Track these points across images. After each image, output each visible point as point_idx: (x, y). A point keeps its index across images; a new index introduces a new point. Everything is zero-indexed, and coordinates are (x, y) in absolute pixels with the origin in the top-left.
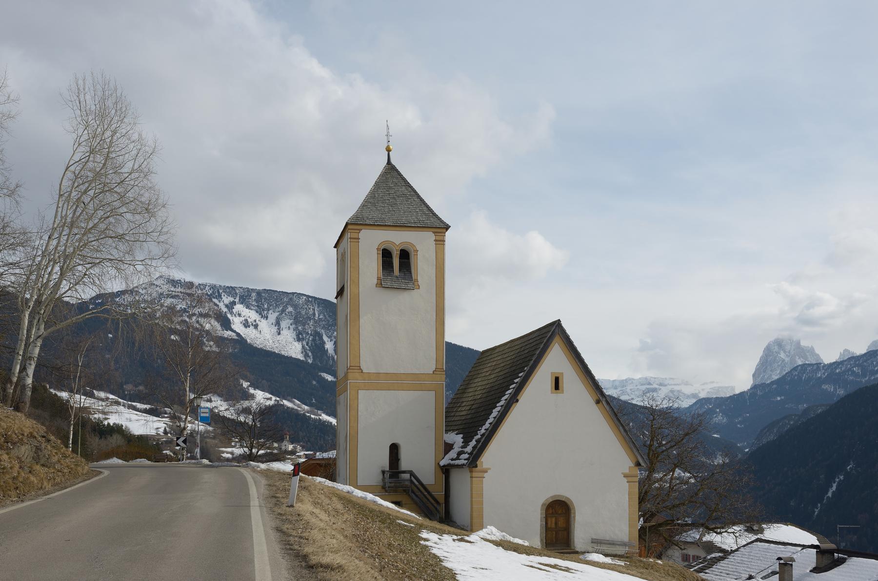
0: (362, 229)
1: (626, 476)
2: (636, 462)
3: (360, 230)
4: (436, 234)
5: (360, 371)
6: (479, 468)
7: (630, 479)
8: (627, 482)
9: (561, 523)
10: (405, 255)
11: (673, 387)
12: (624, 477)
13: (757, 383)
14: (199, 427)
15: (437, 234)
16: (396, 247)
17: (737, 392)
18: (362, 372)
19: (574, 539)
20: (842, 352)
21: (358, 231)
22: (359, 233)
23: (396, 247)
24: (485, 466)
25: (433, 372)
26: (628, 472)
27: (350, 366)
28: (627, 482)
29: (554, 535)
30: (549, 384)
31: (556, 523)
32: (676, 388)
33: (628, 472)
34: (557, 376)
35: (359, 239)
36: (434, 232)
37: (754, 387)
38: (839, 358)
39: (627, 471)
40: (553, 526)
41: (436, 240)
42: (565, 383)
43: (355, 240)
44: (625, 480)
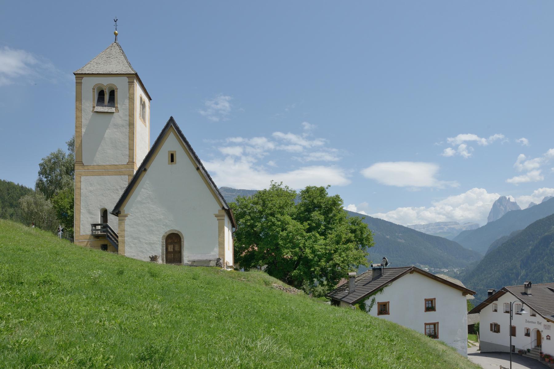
0: (83, 77)
1: (216, 216)
2: (222, 208)
3: (82, 78)
4: (129, 78)
5: (82, 164)
6: (122, 214)
7: (219, 218)
8: (218, 220)
9: (177, 248)
10: (112, 93)
11: (450, 226)
12: (215, 216)
13: (490, 222)
14: (428, 302)
15: (130, 78)
16: (104, 87)
17: (480, 227)
18: (83, 165)
19: (183, 258)
20: (530, 204)
21: (81, 78)
22: (82, 79)
23: (104, 87)
24: (126, 213)
25: (127, 163)
26: (218, 213)
27: (76, 162)
28: (218, 220)
29: (173, 256)
30: (167, 158)
31: (174, 249)
32: (452, 226)
33: (218, 213)
34: (172, 153)
35: (81, 83)
36: (128, 77)
37: (489, 224)
38: (529, 207)
39: (217, 213)
40: (172, 250)
41: (129, 82)
42: (177, 158)
43: (79, 84)
44: (216, 218)
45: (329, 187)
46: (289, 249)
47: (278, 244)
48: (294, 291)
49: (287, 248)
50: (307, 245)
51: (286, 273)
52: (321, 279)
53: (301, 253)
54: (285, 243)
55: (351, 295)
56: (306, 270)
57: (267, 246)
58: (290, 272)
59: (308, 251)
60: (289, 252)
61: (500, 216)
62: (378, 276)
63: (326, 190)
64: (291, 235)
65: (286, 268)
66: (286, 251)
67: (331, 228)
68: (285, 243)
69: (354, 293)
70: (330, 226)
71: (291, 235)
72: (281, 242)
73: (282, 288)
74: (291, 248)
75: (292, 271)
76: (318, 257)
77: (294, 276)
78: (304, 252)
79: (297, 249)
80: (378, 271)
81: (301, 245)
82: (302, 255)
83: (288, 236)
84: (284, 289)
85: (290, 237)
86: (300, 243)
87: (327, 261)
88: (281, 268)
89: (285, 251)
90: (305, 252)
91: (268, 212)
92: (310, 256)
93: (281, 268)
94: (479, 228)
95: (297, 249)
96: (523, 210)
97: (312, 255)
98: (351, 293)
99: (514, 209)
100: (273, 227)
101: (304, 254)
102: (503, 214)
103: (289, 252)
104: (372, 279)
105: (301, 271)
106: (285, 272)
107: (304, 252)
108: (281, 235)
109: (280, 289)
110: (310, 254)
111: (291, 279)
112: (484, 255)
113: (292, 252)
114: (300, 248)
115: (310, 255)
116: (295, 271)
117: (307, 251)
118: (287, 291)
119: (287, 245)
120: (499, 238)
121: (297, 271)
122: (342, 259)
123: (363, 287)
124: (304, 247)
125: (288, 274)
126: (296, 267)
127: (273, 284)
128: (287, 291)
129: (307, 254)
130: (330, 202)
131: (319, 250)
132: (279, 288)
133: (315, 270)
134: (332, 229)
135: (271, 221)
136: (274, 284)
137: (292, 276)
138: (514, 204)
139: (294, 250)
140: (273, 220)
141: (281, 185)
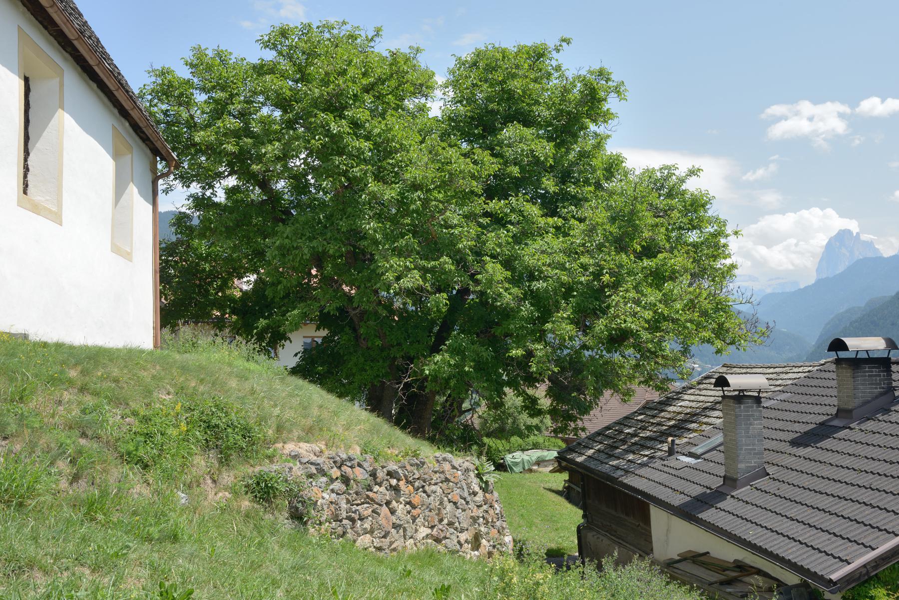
17: (802, 287)
37: (819, 282)
45: (564, 44)
46: (409, 256)
47: (357, 234)
48: (447, 480)
49: (399, 253)
50: (490, 245)
51: (399, 362)
52: (530, 391)
53: (465, 278)
54: (392, 231)
55: (742, 492)
56: (487, 353)
57: (310, 241)
58: (415, 361)
59: (495, 270)
60: (408, 269)
61: (841, 269)
62: (877, 397)
63: (554, 54)
64: (420, 199)
65: (399, 344)
66: (395, 262)
67: (574, 197)
68: (392, 231)
69: (758, 483)
70: (572, 189)
71: (420, 199)
72: (370, 226)
73: (360, 474)
74: (418, 253)
75: (425, 357)
76: (532, 305)
77: (435, 377)
78: (479, 277)
79: (447, 262)
80: (875, 371)
81: (464, 244)
82: (472, 288)
83: (402, 202)
84: (373, 475)
85: (413, 207)
86: (459, 238)
87: (582, 321)
88: (379, 342)
89: (392, 266)
90: (479, 273)
91: (314, 93)
92: (508, 296)
93: (379, 342)
94: (800, 289)
95: (447, 262)
96: (888, 258)
97: (515, 290)
98: (748, 482)
99: (870, 255)
100: (337, 160)
101: (477, 282)
102: (847, 263)
103: (408, 269)
104: (834, 411)
105: (463, 358)
106: (395, 358)
107: (479, 277)
108: (373, 196)
109: (346, 480)
110: (507, 285)
111: (422, 388)
112: (814, 343)
113: (424, 271)
114: (460, 261)
115: (506, 290)
116: (438, 358)
117: (490, 271)
118: (396, 489)
119: (402, 242)
120: (841, 311)
121: (447, 356)
122: (648, 314)
123: (794, 450)
124: (478, 253)
125: (407, 370)
126: (441, 339)
127: (290, 447)
128: (396, 489)
129: (490, 282)
130: (576, 93)
131: (541, 272)
132: (335, 472)
133: (530, 354)
134: (580, 200)
135: (328, 133)
136: (300, 439)
137: (427, 377)
138: (869, 245)
139: (433, 263)
140: (334, 128)
141: (377, 39)
